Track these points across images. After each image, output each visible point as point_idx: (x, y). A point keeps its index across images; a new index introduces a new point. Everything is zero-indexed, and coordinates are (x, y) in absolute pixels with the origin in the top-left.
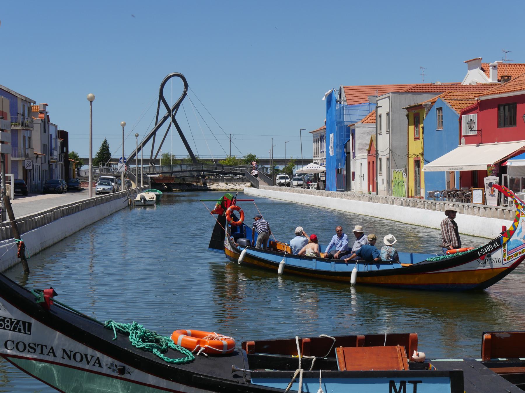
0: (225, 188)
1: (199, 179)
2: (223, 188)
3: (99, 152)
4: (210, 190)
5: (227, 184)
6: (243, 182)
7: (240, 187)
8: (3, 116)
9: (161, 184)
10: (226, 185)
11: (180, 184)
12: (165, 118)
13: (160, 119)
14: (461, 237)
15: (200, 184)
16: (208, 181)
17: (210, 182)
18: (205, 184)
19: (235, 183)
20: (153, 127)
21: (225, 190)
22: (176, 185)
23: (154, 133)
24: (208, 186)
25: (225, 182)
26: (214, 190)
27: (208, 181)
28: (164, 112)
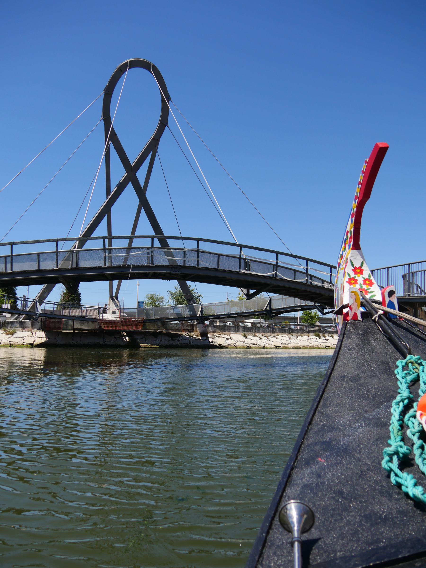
0: (242, 344)
1: (192, 325)
2: (239, 344)
3: (16, 291)
4: (215, 347)
5: (245, 336)
6: (273, 332)
7: (270, 343)
8: (425, 437)
9: (119, 332)
10: (243, 338)
11: (155, 334)
12: (121, 187)
13: (113, 189)
14: (37, 260)
15: (196, 335)
16: (210, 329)
17: (215, 332)
18: (204, 334)
19: (260, 335)
20: (104, 200)
21: (243, 347)
22: (146, 335)
23: (106, 211)
24: (211, 340)
25: (241, 332)
26: (220, 346)
27: (210, 329)
28: (119, 173)
